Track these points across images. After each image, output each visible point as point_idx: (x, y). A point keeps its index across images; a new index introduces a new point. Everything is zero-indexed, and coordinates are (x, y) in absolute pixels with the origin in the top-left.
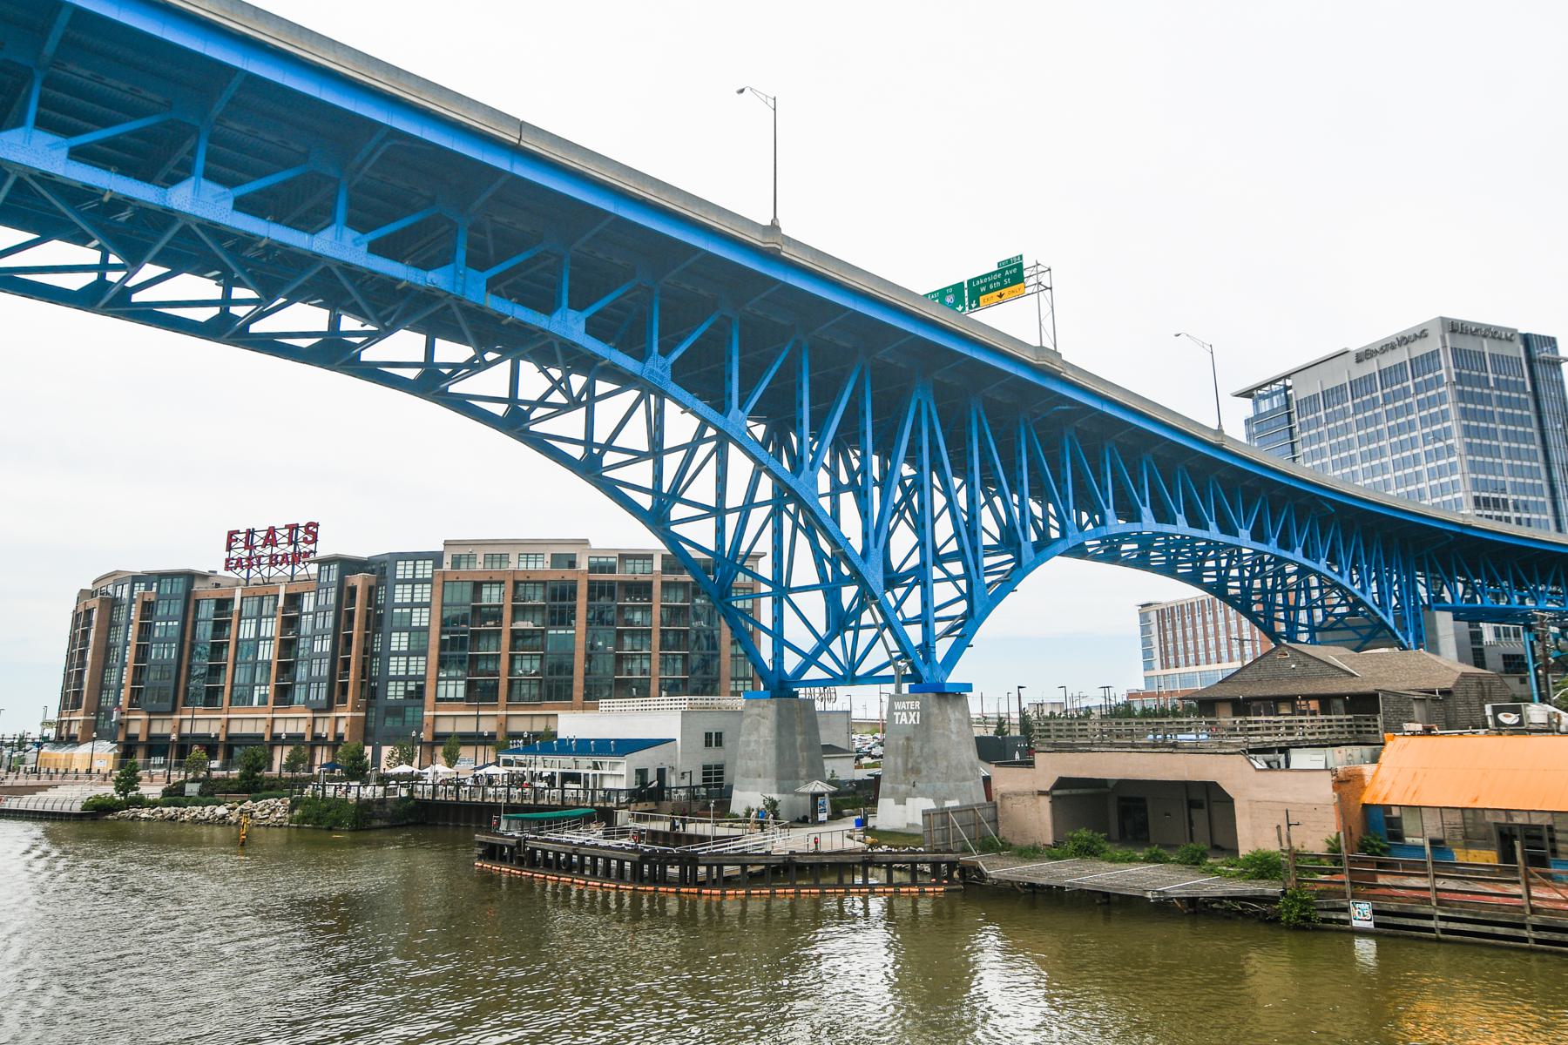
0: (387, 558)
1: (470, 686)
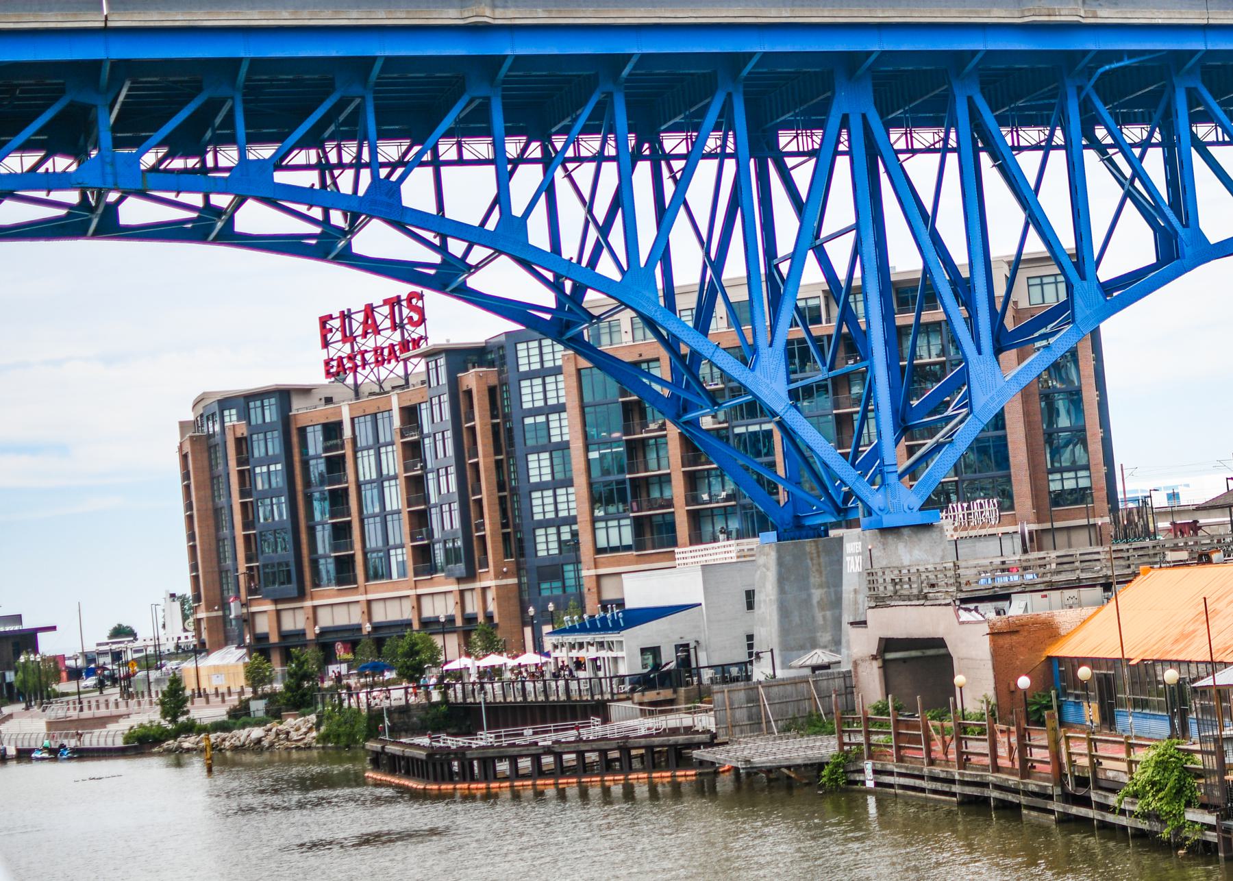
0: (503, 338)
1: (639, 526)
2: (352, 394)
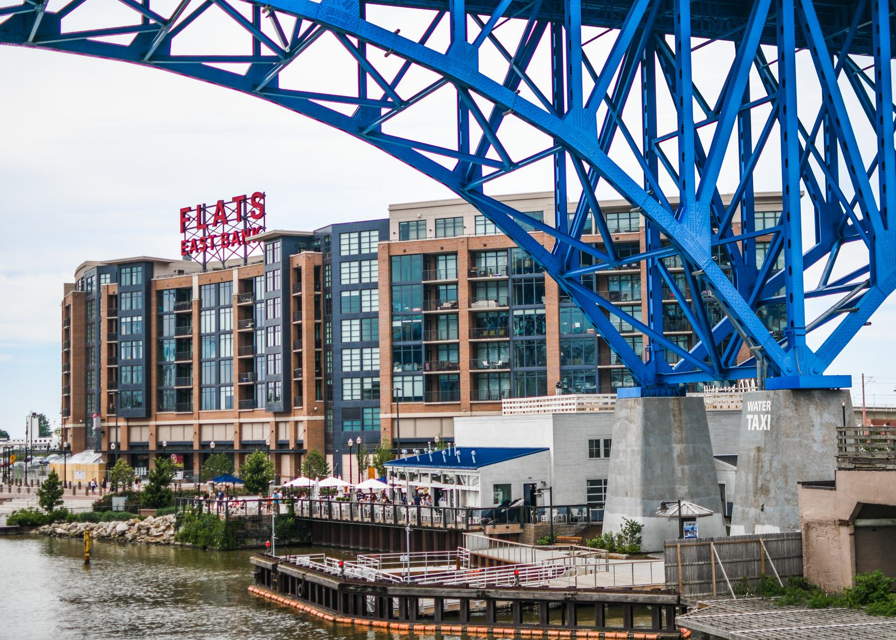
0: (330, 230)
1: (430, 382)
2: (201, 267)
